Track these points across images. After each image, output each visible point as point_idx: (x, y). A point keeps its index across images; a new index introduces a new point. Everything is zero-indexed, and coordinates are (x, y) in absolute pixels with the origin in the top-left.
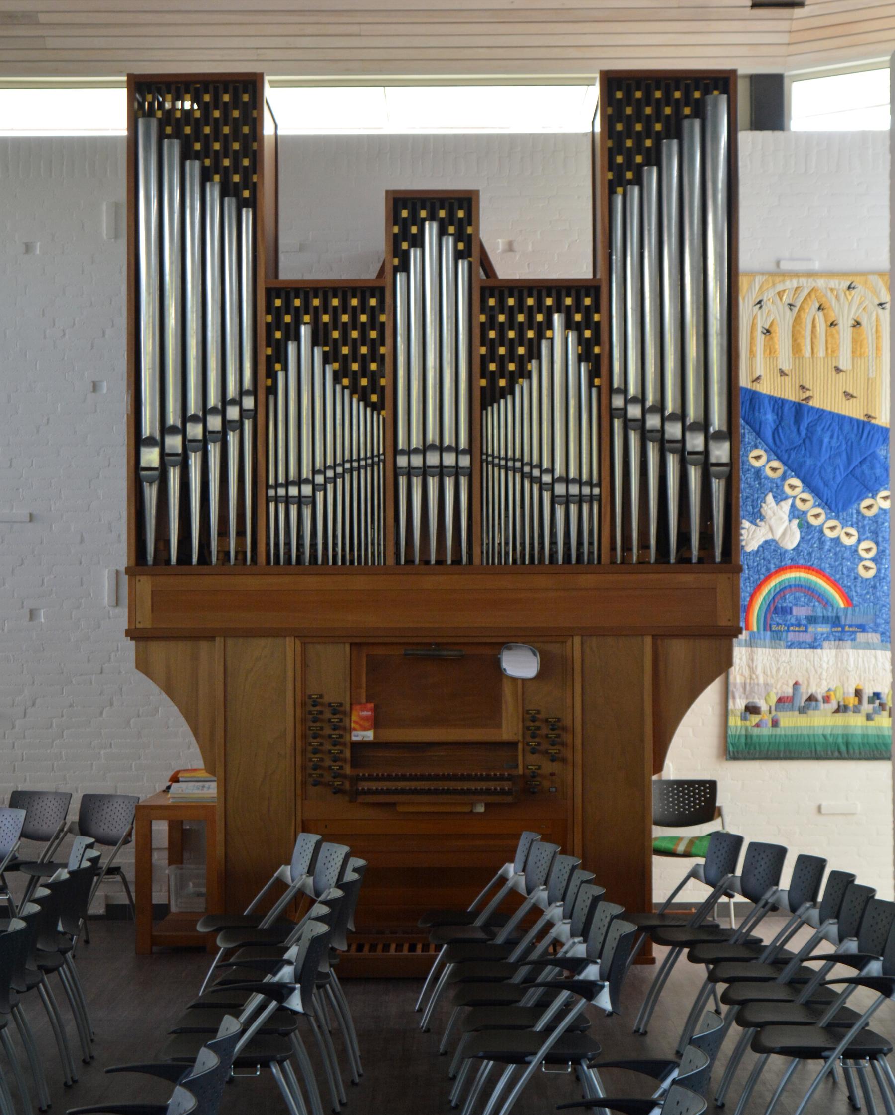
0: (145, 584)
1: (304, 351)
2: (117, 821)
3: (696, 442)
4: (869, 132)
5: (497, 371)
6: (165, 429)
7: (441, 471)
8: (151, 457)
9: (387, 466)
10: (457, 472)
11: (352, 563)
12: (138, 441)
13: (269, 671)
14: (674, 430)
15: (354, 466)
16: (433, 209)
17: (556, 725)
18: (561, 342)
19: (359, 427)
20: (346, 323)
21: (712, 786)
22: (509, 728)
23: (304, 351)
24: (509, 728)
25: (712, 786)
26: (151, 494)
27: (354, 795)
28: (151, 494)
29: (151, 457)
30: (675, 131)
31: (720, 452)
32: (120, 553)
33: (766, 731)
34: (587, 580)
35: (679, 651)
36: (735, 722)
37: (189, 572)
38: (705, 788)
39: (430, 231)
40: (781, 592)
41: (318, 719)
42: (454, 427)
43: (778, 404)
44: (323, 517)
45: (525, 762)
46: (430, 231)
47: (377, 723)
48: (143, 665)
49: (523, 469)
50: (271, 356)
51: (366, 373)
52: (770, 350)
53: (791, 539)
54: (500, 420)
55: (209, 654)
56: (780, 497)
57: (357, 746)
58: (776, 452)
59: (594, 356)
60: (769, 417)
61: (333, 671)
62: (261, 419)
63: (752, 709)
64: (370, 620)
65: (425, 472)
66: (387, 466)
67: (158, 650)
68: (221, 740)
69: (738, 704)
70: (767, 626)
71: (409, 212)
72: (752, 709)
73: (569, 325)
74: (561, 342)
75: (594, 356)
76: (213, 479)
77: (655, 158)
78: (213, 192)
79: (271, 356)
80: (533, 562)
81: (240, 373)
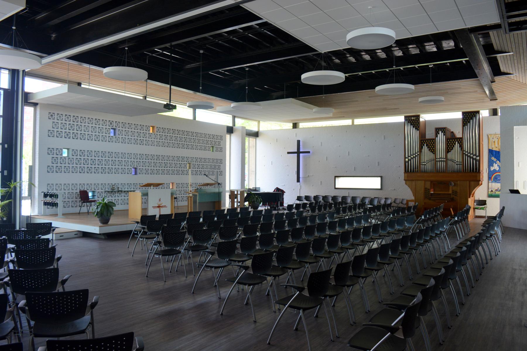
0: (406, 174)
1: (425, 148)
2: (405, 202)
3: (475, 157)
4: (247, 103)
5: (449, 148)
6: (409, 156)
7: (442, 161)
8: (407, 160)
9: (435, 161)
10: (444, 161)
11: (431, 172)
12: (405, 158)
13: (421, 184)
14: (469, 155)
15: (431, 161)
16: (441, 129)
17: (456, 192)
18: (457, 145)
19: (432, 156)
20: (431, 144)
21: (486, 201)
22: (450, 192)
23: (425, 148)
24: (450, 192)
25: (486, 201)
26: (407, 164)
27: (430, 199)
28: (407, 164)
29: (407, 160)
30: (472, 119)
31: (478, 158)
32: (403, 171)
33: (494, 194)
34: (460, 174)
35: (472, 183)
36: (489, 193)
37: (411, 173)
38: (50, 252)
39: (440, 132)
40: (496, 176)
41: (426, 190)
42: (443, 156)
43: (496, 151)
44: (429, 167)
45: (452, 196)
46: (440, 132)
47: (434, 191)
48: (406, 184)
49: (452, 161)
50: (421, 148)
51: (432, 148)
52: (495, 144)
53: (498, 169)
54: (449, 155)
55: (414, 183)
56: (496, 163)
57: (431, 194)
58: (495, 157)
59: (461, 146)
60: (494, 153)
61: (428, 185)
62: (420, 155)
63: (492, 191)
64: (433, 179)
65: (440, 161)
66: (435, 161)
67: (408, 182)
68: (415, 193)
69: (490, 190)
70: (494, 180)
71: (437, 130)
72: (492, 191)
73: (458, 143)
74: (457, 145)
75: (461, 146)
76: (414, 162)
77: (469, 122)
78: (414, 129)
79: (421, 148)
80: (453, 172)
81: (417, 149)
